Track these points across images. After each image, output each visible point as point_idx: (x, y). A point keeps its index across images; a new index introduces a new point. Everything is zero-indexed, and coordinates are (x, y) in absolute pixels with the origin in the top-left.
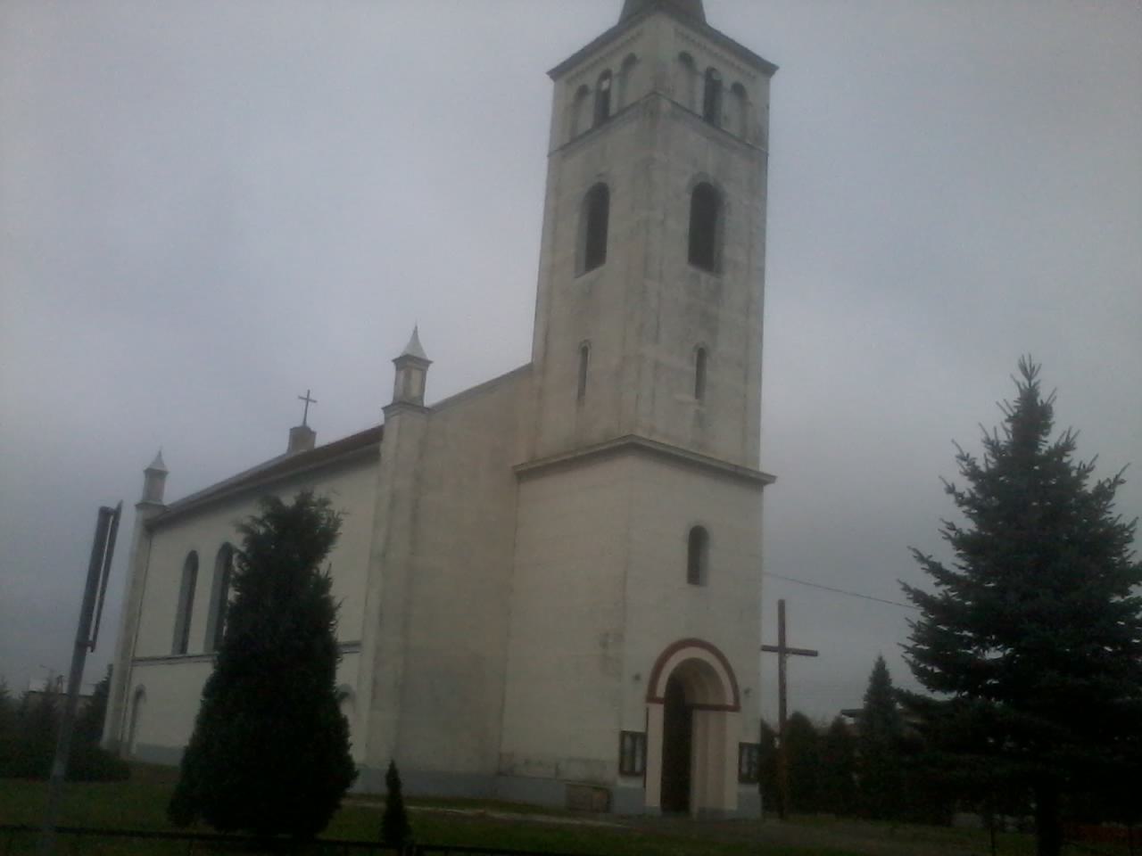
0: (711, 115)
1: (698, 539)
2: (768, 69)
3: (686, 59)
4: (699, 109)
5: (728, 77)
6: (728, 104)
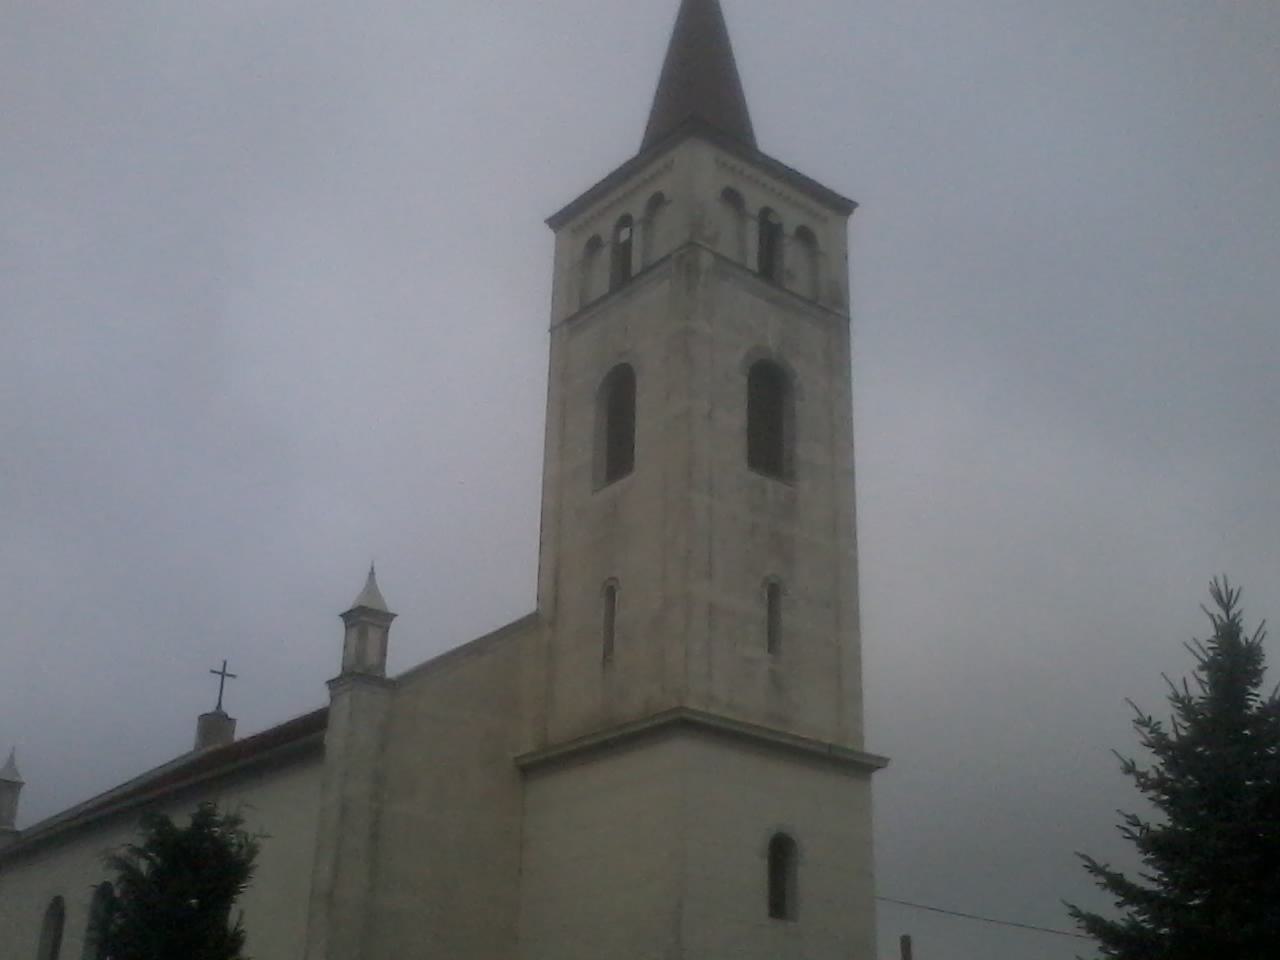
0: (769, 269)
1: (781, 852)
2: (844, 207)
3: (731, 197)
4: (753, 263)
5: (790, 220)
6: (792, 255)
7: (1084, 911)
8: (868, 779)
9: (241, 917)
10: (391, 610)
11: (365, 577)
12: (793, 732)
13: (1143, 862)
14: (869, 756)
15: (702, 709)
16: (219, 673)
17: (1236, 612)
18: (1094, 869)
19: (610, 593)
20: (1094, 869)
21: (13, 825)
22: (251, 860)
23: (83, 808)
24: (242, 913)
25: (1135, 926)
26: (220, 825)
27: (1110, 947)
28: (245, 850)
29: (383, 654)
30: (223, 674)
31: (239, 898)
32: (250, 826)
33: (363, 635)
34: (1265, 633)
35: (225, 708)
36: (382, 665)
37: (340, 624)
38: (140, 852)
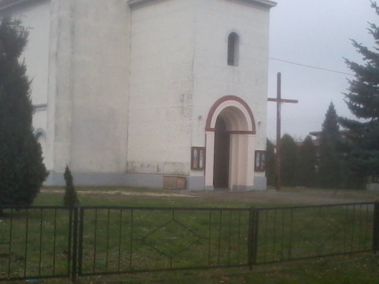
7: (350, 61)
8: (269, 11)
9: (24, 60)
13: (375, 43)
17: (361, 56)
18: (356, 45)
20: (356, 45)
22: (26, 38)
24: (24, 58)
25: (43, 173)
26: (12, 24)
27: (359, 75)
28: (23, 34)
31: (23, 53)
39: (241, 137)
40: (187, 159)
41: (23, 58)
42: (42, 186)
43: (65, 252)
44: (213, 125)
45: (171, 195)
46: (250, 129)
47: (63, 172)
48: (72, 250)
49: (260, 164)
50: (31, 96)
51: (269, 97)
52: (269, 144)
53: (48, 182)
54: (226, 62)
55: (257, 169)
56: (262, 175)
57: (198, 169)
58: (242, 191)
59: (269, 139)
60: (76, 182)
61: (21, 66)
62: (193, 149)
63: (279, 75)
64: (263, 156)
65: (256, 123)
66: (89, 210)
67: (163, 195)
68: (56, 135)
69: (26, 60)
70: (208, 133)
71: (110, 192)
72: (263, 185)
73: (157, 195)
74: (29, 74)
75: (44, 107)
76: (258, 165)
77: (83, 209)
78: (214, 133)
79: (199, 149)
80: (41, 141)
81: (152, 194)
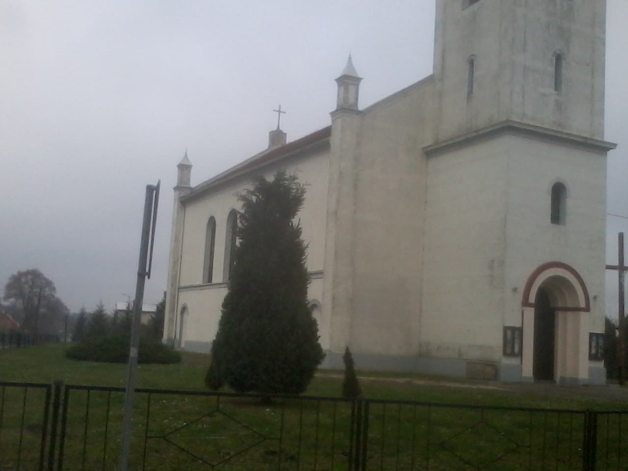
1: (558, 192)
8: (606, 155)
10: (360, 76)
11: (347, 59)
12: (568, 132)
14: (606, 143)
15: (519, 121)
16: (277, 111)
19: (471, 63)
21: (189, 184)
23: (216, 179)
25: (318, 355)
26: (286, 180)
29: (357, 99)
30: (279, 111)
32: (302, 179)
33: (346, 90)
34: (184, 309)
35: (281, 128)
36: (356, 104)
37: (335, 84)
38: (253, 193)
39: (570, 315)
40: (496, 340)
41: (298, 219)
42: (317, 370)
43: (344, 454)
44: (532, 299)
45: (476, 387)
46: (583, 304)
47: (344, 352)
48: (354, 451)
49: (597, 351)
50: (306, 264)
51: (609, 263)
52: (608, 323)
53: (325, 365)
54: (549, 220)
55: (593, 357)
56: (601, 365)
57: (512, 354)
58: (573, 385)
59: (609, 317)
60: (357, 367)
61: (244, 208)
62: (506, 329)
63: (621, 237)
64: (601, 341)
65: (591, 298)
66: (12, 388)
67: (466, 386)
68: (333, 308)
69: (301, 220)
70: (525, 308)
71: (398, 380)
72: (602, 379)
73: (458, 385)
74: (304, 237)
75: (320, 273)
76: (593, 351)
77: (368, 402)
78: (533, 309)
79: (513, 329)
80: (315, 315)
81: (453, 385)
